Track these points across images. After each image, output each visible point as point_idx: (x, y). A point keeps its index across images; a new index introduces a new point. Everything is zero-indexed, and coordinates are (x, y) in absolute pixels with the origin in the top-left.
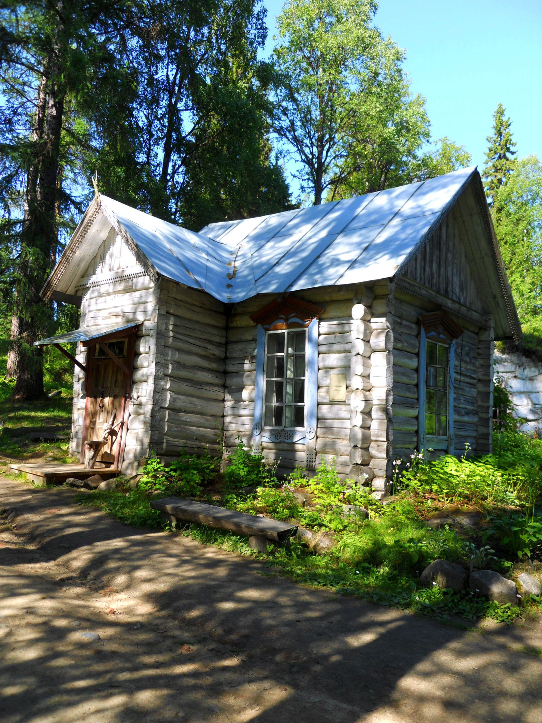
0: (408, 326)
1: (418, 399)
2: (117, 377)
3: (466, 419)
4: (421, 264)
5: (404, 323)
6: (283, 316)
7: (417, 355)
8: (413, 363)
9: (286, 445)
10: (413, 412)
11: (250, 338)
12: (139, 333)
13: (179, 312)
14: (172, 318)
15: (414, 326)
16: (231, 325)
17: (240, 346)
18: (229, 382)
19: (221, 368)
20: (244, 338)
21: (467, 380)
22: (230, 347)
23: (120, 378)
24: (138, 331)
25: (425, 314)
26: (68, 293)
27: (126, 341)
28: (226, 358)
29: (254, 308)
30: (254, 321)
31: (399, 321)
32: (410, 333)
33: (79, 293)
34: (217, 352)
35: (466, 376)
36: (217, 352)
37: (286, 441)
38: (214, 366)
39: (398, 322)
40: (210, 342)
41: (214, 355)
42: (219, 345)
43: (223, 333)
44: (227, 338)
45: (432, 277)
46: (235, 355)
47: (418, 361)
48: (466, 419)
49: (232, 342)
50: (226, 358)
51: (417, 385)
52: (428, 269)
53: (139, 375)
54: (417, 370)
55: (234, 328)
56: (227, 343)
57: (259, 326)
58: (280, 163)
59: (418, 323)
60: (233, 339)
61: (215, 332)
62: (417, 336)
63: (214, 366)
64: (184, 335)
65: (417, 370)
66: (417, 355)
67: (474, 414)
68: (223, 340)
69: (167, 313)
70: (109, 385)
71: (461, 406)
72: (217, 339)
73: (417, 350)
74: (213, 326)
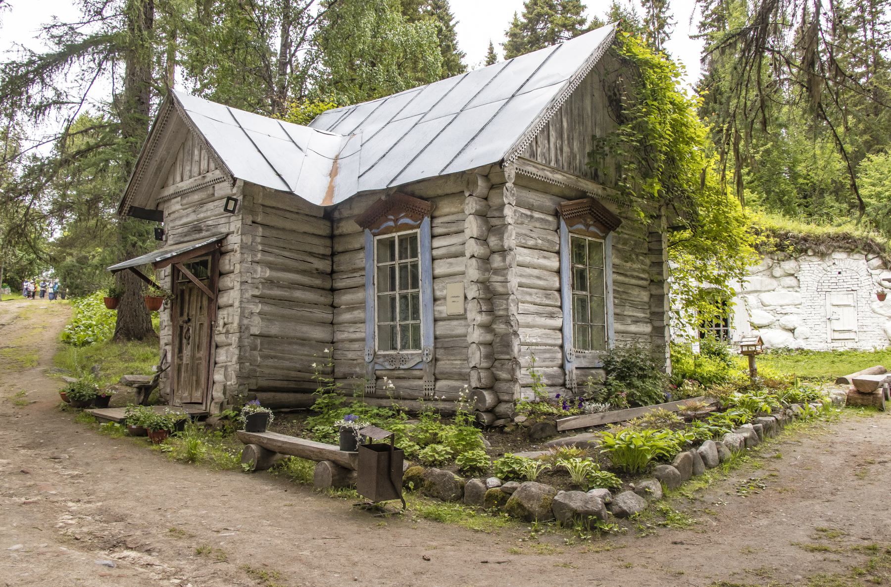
0: (542, 219)
1: (561, 307)
2: (201, 302)
3: (633, 328)
4: (555, 144)
5: (537, 215)
6: (392, 217)
7: (558, 253)
8: (554, 263)
9: (402, 372)
10: (557, 323)
11: (357, 246)
12: (223, 249)
13: (268, 221)
14: (260, 229)
15: (550, 218)
16: (337, 232)
17: (347, 257)
18: (337, 301)
19: (328, 285)
20: (351, 247)
21: (633, 281)
22: (336, 259)
23: (205, 303)
24: (222, 246)
25: (564, 202)
26: (148, 208)
27: (210, 258)
28: (333, 272)
29: (359, 209)
30: (361, 225)
31: (528, 213)
32: (546, 227)
33: (160, 208)
34: (323, 265)
35: (633, 277)
36: (323, 265)
37: (402, 367)
38: (317, 282)
39: (527, 215)
40: (311, 254)
41: (317, 270)
42: (323, 257)
43: (328, 242)
44: (332, 248)
45: (574, 158)
46: (342, 268)
47: (560, 261)
48: (633, 328)
49: (339, 253)
50: (333, 272)
51: (559, 290)
52: (566, 149)
53: (223, 300)
54: (559, 272)
55: (341, 235)
56: (333, 254)
57: (367, 230)
58: (606, 19)
59: (557, 214)
60: (340, 249)
61: (316, 241)
62: (556, 231)
63: (317, 282)
64: (278, 247)
65: (559, 272)
66: (558, 253)
67: (647, 323)
68: (328, 252)
69: (253, 222)
70: (194, 313)
71: (626, 313)
72: (322, 251)
73: (557, 248)
74: (313, 234)
